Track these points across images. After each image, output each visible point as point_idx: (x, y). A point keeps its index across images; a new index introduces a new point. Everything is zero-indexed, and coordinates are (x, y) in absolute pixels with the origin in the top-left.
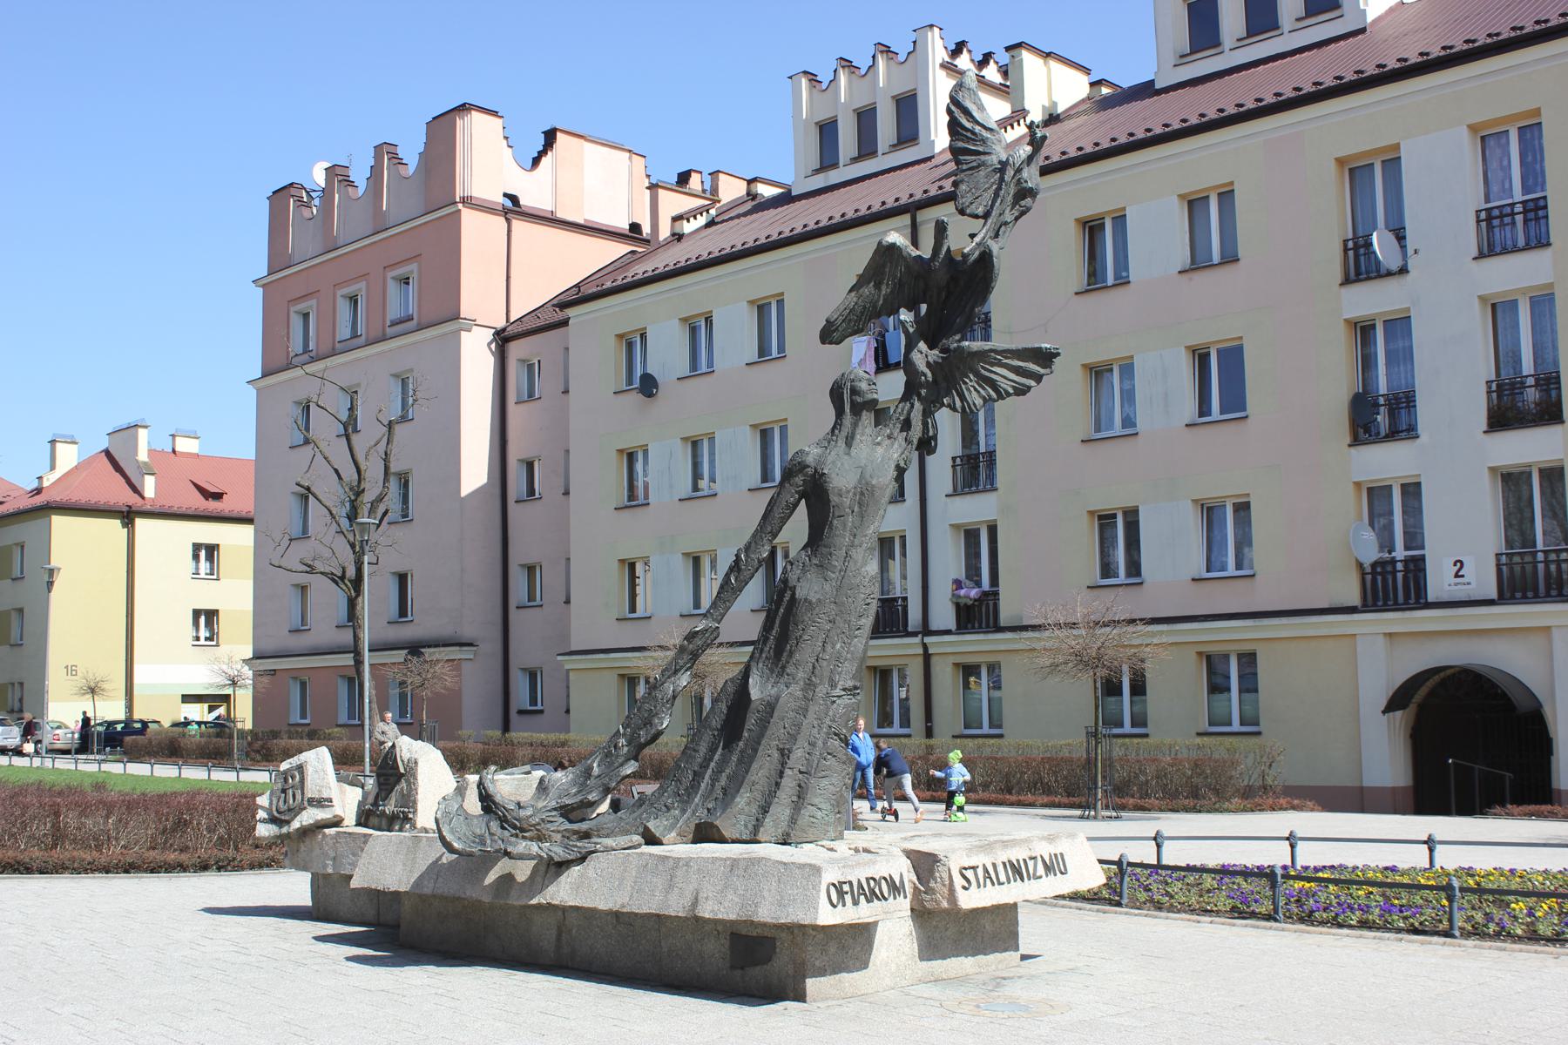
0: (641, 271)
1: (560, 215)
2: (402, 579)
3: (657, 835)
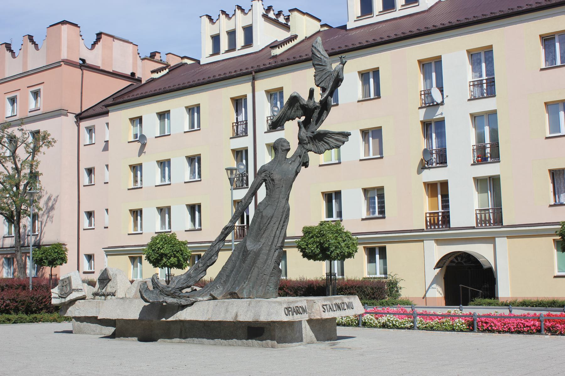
0: (140, 93)
3: (216, 297)
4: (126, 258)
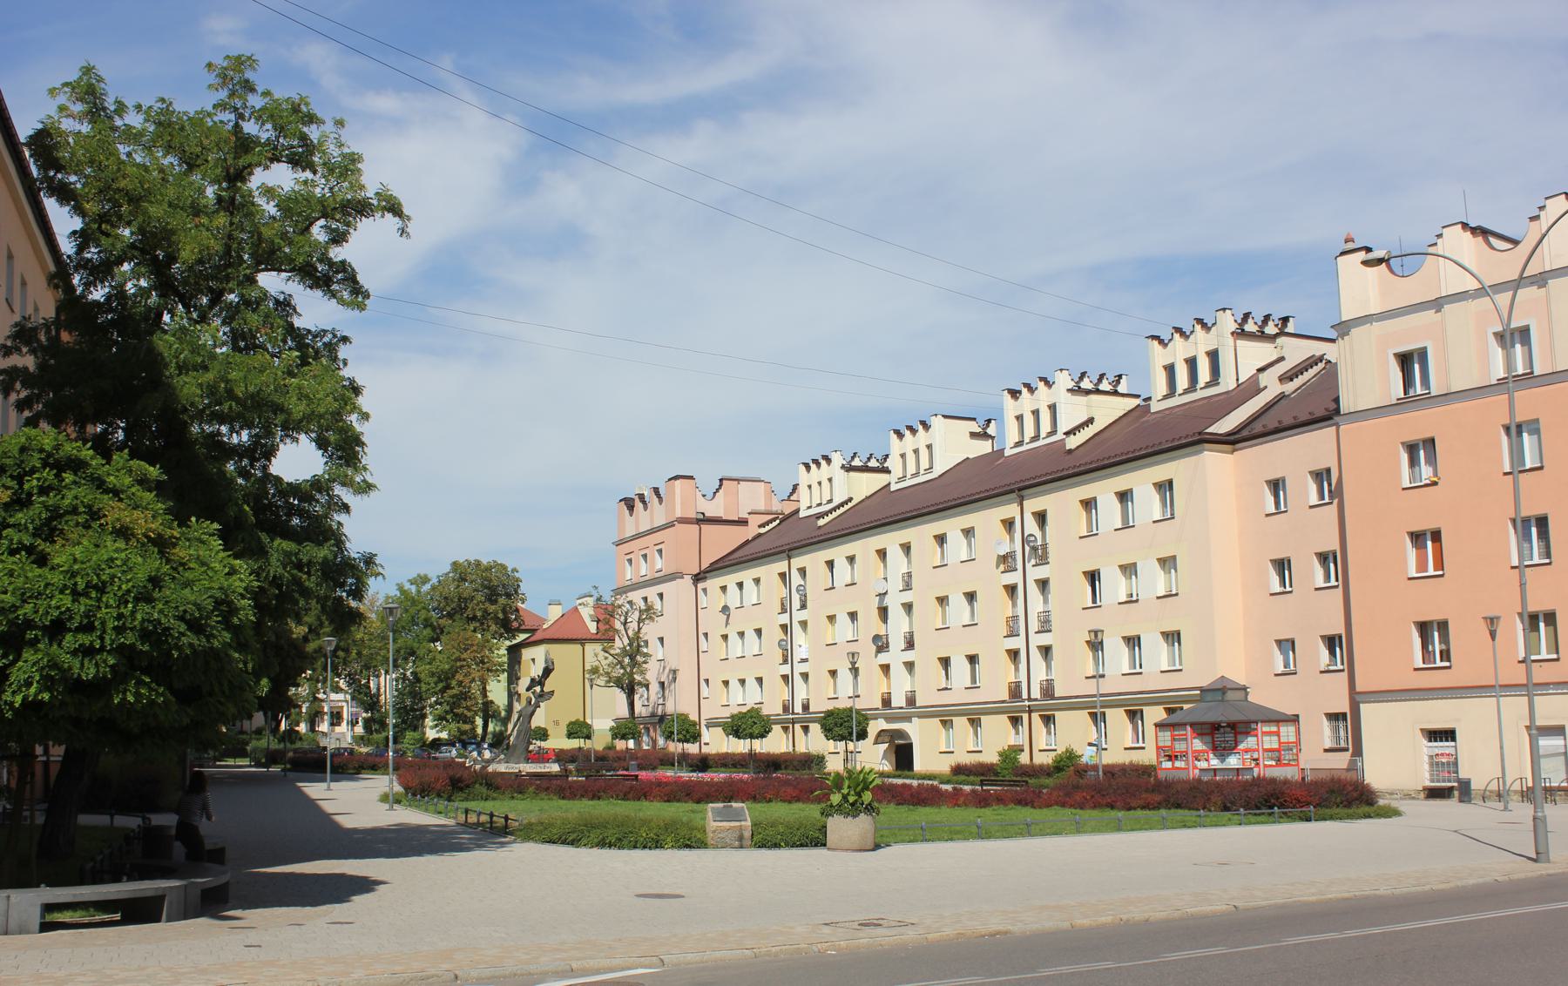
4: (1084, 715)
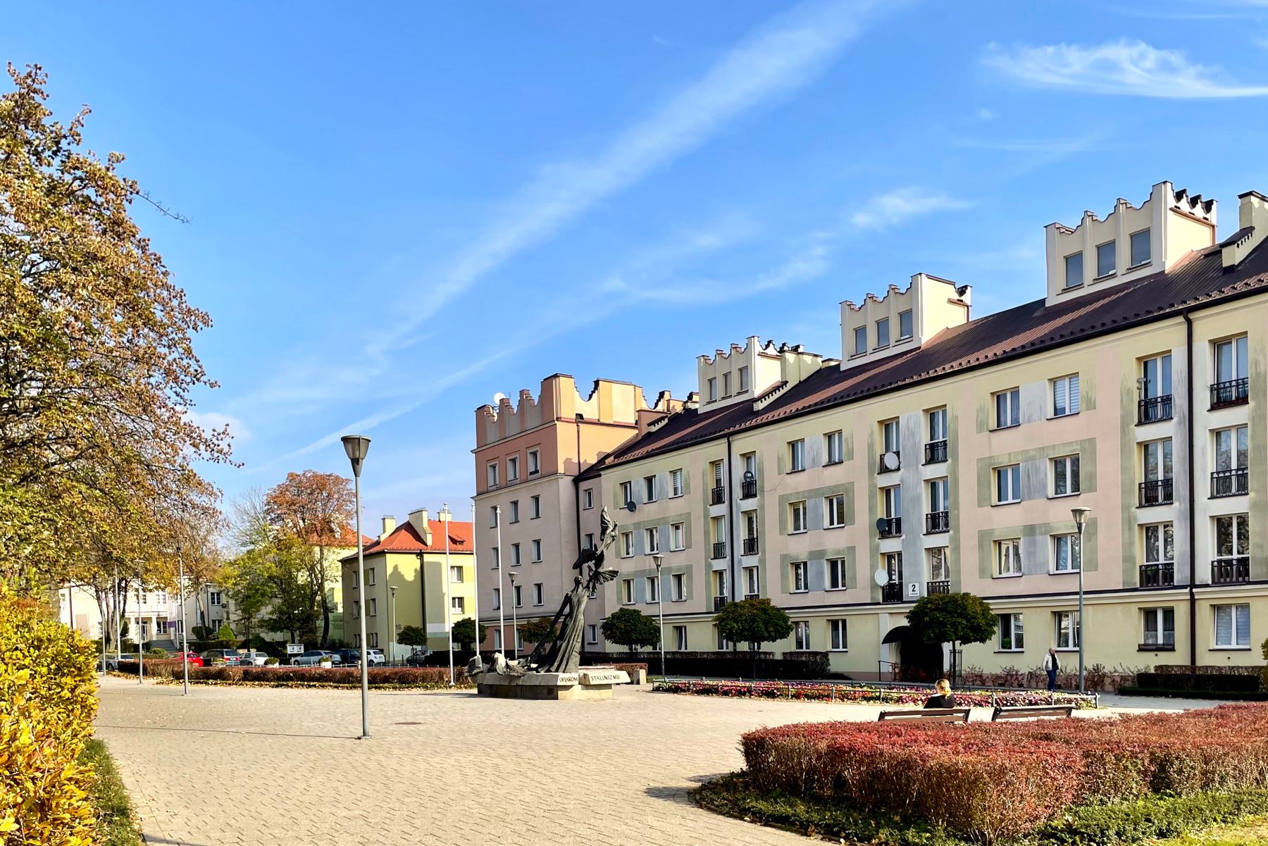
1: (602, 421)
2: (539, 586)
